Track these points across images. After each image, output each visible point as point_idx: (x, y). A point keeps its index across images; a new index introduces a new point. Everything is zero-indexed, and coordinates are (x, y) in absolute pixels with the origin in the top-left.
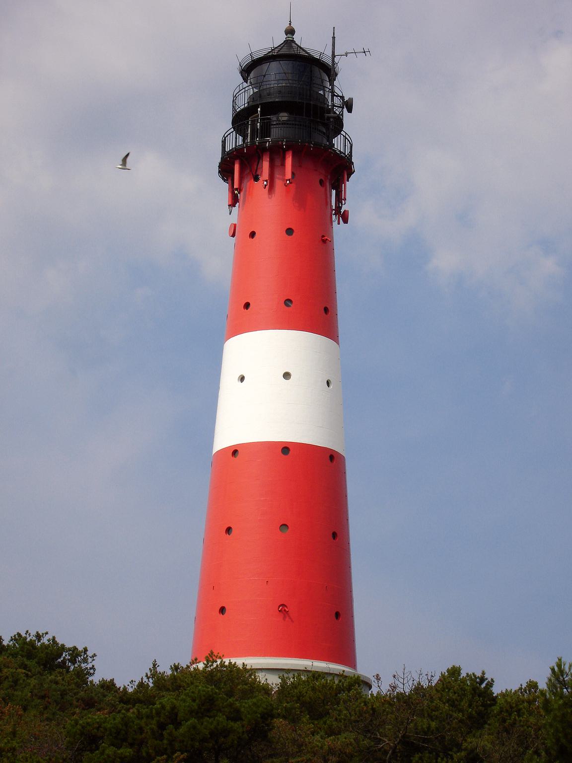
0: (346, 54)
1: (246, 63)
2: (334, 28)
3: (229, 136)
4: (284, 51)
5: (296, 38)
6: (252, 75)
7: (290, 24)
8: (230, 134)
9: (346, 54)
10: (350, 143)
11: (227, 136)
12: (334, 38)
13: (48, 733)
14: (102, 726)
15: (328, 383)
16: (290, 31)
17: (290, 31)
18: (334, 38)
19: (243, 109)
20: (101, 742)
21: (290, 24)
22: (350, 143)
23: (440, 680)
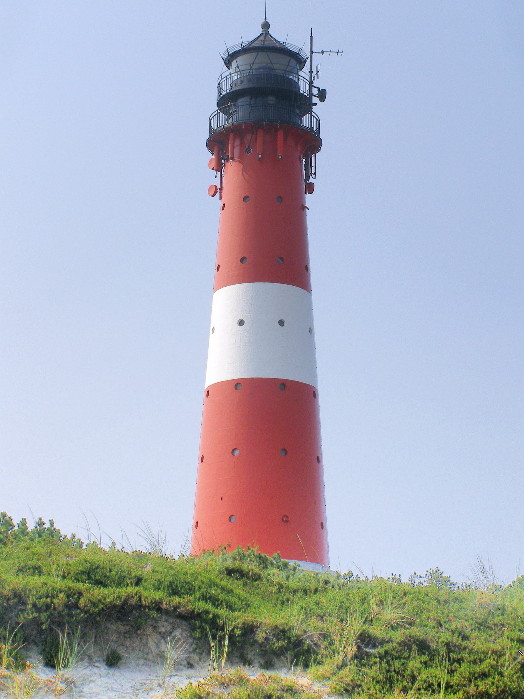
0: (323, 52)
1: (233, 52)
2: (311, 29)
3: (214, 117)
4: (257, 44)
5: (270, 31)
6: (234, 65)
7: (266, 19)
8: (215, 115)
9: (323, 52)
10: (317, 119)
11: (212, 118)
12: (311, 37)
13: (431, 633)
14: (450, 633)
15: (281, 323)
16: (266, 25)
17: (266, 25)
18: (311, 37)
19: (224, 95)
20: (128, 636)
21: (266, 19)
22: (317, 119)
23: (124, 600)
